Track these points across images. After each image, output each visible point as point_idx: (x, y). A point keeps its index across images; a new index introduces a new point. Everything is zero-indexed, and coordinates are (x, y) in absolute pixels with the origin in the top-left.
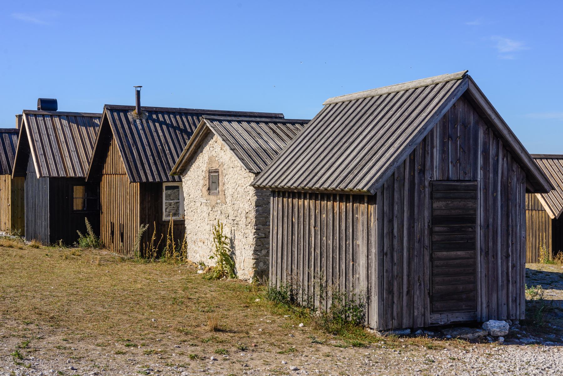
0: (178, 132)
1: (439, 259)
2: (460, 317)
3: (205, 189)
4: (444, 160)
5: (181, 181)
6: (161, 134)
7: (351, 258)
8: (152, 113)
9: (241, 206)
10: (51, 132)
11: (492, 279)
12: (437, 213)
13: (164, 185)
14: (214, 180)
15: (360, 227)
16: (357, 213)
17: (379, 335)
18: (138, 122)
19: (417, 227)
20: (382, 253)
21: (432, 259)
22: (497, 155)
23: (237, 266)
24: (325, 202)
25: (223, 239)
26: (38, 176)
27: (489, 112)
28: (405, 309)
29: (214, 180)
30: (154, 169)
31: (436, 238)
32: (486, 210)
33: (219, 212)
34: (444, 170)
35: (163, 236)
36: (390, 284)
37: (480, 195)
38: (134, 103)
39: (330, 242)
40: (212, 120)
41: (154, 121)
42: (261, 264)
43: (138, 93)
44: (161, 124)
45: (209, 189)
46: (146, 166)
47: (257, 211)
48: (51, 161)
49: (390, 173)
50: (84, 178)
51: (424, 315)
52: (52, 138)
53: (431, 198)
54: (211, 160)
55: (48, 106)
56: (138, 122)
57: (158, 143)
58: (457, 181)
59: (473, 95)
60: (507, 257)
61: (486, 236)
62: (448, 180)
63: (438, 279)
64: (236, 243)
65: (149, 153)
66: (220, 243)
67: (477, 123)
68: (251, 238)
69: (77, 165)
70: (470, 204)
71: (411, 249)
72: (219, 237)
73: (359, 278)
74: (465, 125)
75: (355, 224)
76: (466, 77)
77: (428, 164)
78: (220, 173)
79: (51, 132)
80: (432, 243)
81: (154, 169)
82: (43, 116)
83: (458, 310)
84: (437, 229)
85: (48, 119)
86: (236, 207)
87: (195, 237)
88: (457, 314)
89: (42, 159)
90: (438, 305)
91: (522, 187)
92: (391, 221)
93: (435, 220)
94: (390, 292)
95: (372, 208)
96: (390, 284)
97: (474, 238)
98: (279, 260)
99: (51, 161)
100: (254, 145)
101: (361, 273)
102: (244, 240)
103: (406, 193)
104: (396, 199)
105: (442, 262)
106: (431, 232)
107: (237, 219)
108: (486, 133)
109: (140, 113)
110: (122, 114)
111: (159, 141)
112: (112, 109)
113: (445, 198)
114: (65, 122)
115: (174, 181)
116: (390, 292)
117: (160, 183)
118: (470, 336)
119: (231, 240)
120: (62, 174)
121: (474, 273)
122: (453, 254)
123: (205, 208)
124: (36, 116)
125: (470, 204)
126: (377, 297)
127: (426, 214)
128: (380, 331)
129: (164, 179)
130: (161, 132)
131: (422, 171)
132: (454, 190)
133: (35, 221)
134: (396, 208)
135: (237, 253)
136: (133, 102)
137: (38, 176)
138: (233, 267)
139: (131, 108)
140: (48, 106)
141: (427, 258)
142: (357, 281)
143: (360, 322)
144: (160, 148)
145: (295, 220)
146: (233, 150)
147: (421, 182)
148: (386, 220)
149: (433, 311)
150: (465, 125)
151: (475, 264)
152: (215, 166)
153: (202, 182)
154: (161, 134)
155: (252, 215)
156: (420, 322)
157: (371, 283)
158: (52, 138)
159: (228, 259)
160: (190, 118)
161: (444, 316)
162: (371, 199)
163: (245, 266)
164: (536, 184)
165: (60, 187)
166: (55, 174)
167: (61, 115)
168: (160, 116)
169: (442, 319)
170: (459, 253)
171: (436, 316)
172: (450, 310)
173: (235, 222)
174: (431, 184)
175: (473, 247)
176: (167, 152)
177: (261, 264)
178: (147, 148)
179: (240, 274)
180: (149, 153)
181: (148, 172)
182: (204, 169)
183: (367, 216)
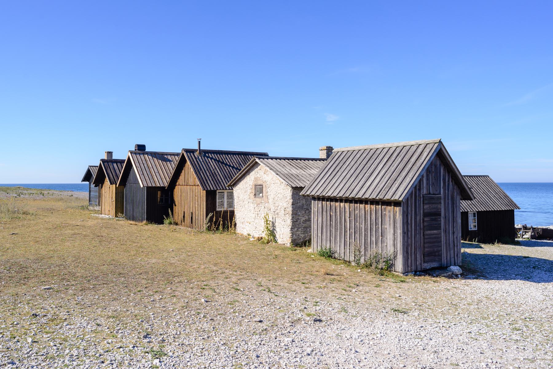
0: (238, 164)
1: (427, 235)
2: (435, 265)
3: (252, 196)
4: (428, 184)
5: (232, 189)
6: (212, 164)
7: (380, 234)
8: (205, 153)
9: (281, 204)
10: (144, 162)
11: (448, 244)
12: (426, 211)
13: (217, 191)
14: (259, 190)
15: (387, 219)
16: (385, 211)
17: (402, 275)
18: (200, 157)
19: (418, 218)
20: (404, 233)
21: (424, 235)
22: (449, 181)
23: (277, 236)
24: (380, 206)
25: (268, 222)
26: (142, 186)
27: (449, 159)
28: (413, 261)
29: (259, 190)
30: (212, 183)
31: (426, 224)
32: (445, 209)
33: (263, 207)
34: (428, 189)
35: (221, 219)
36: (407, 248)
37: (442, 202)
38: (197, 148)
39: (363, 226)
40: (259, 158)
41: (208, 157)
42: (294, 236)
43: (199, 142)
44: (211, 159)
45: (255, 195)
46: (208, 181)
47: (293, 207)
48: (147, 178)
49: (410, 191)
50: (164, 187)
51: (421, 264)
52: (145, 165)
53: (423, 203)
54: (256, 179)
55: (141, 148)
56: (200, 157)
57: (212, 169)
58: (434, 194)
59: (443, 153)
60: (454, 233)
61: (445, 223)
62: (430, 194)
63: (426, 245)
64: (276, 224)
65: (208, 175)
66: (267, 224)
67: (440, 165)
68: (289, 222)
69: (162, 179)
70: (439, 206)
71: (415, 230)
72: (267, 221)
73: (386, 246)
74: (436, 166)
75: (383, 217)
76: (440, 142)
77: (422, 187)
78: (264, 186)
79: (144, 162)
80: (424, 226)
81: (212, 183)
82: (139, 154)
83: (435, 261)
84: (426, 219)
85: (142, 156)
86: (277, 205)
87: (243, 220)
88: (434, 263)
89: (142, 177)
90: (426, 258)
91: (459, 197)
92: (407, 216)
93: (426, 215)
94: (407, 253)
95: (397, 209)
96: (407, 248)
97: (441, 224)
98: (320, 235)
99: (147, 178)
100: (286, 172)
101: (388, 243)
102: (283, 223)
103: (413, 201)
104: (409, 205)
105: (428, 237)
106: (424, 221)
107: (277, 211)
108: (444, 170)
109: (200, 153)
110: (192, 154)
111: (222, 169)
112: (187, 151)
113: (429, 203)
114: (150, 157)
115: (229, 189)
116: (407, 253)
117: (216, 191)
118: (445, 274)
119: (273, 222)
120: (154, 185)
121: (441, 242)
122: (433, 232)
123: (252, 205)
124: (135, 153)
125: (439, 206)
126: (401, 256)
127: (422, 212)
128: (403, 274)
129: (218, 188)
130: (212, 163)
131: (420, 190)
132: (431, 199)
133: (133, 210)
134: (409, 209)
135: (277, 229)
136: (197, 147)
137: (142, 186)
138: (274, 237)
139: (196, 150)
140: (141, 148)
141: (422, 234)
142: (385, 247)
143: (390, 266)
144: (213, 171)
145: (333, 214)
146: (277, 174)
147: (419, 195)
148: (405, 215)
149: (424, 262)
150: (436, 166)
151: (441, 237)
152: (260, 183)
153: (249, 191)
154: (212, 164)
155: (290, 209)
156: (419, 269)
157: (397, 248)
158: (145, 165)
159: (272, 233)
160: (224, 155)
161: (429, 264)
162: (397, 204)
163: (284, 235)
164: (466, 195)
165: (151, 191)
166: (150, 185)
167: (148, 153)
168: (210, 155)
169: (427, 266)
170: (435, 231)
171: (426, 264)
172: (432, 261)
173: (276, 213)
174: (423, 196)
175: (439, 228)
176: (217, 174)
177: (294, 236)
178: (207, 172)
179: (280, 241)
180: (208, 175)
181: (210, 184)
182: (251, 184)
183: (395, 214)
